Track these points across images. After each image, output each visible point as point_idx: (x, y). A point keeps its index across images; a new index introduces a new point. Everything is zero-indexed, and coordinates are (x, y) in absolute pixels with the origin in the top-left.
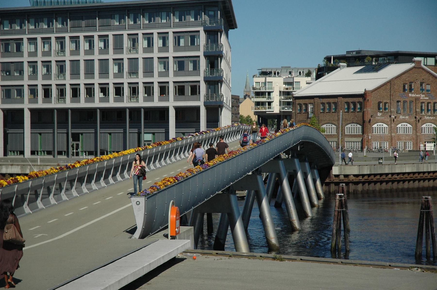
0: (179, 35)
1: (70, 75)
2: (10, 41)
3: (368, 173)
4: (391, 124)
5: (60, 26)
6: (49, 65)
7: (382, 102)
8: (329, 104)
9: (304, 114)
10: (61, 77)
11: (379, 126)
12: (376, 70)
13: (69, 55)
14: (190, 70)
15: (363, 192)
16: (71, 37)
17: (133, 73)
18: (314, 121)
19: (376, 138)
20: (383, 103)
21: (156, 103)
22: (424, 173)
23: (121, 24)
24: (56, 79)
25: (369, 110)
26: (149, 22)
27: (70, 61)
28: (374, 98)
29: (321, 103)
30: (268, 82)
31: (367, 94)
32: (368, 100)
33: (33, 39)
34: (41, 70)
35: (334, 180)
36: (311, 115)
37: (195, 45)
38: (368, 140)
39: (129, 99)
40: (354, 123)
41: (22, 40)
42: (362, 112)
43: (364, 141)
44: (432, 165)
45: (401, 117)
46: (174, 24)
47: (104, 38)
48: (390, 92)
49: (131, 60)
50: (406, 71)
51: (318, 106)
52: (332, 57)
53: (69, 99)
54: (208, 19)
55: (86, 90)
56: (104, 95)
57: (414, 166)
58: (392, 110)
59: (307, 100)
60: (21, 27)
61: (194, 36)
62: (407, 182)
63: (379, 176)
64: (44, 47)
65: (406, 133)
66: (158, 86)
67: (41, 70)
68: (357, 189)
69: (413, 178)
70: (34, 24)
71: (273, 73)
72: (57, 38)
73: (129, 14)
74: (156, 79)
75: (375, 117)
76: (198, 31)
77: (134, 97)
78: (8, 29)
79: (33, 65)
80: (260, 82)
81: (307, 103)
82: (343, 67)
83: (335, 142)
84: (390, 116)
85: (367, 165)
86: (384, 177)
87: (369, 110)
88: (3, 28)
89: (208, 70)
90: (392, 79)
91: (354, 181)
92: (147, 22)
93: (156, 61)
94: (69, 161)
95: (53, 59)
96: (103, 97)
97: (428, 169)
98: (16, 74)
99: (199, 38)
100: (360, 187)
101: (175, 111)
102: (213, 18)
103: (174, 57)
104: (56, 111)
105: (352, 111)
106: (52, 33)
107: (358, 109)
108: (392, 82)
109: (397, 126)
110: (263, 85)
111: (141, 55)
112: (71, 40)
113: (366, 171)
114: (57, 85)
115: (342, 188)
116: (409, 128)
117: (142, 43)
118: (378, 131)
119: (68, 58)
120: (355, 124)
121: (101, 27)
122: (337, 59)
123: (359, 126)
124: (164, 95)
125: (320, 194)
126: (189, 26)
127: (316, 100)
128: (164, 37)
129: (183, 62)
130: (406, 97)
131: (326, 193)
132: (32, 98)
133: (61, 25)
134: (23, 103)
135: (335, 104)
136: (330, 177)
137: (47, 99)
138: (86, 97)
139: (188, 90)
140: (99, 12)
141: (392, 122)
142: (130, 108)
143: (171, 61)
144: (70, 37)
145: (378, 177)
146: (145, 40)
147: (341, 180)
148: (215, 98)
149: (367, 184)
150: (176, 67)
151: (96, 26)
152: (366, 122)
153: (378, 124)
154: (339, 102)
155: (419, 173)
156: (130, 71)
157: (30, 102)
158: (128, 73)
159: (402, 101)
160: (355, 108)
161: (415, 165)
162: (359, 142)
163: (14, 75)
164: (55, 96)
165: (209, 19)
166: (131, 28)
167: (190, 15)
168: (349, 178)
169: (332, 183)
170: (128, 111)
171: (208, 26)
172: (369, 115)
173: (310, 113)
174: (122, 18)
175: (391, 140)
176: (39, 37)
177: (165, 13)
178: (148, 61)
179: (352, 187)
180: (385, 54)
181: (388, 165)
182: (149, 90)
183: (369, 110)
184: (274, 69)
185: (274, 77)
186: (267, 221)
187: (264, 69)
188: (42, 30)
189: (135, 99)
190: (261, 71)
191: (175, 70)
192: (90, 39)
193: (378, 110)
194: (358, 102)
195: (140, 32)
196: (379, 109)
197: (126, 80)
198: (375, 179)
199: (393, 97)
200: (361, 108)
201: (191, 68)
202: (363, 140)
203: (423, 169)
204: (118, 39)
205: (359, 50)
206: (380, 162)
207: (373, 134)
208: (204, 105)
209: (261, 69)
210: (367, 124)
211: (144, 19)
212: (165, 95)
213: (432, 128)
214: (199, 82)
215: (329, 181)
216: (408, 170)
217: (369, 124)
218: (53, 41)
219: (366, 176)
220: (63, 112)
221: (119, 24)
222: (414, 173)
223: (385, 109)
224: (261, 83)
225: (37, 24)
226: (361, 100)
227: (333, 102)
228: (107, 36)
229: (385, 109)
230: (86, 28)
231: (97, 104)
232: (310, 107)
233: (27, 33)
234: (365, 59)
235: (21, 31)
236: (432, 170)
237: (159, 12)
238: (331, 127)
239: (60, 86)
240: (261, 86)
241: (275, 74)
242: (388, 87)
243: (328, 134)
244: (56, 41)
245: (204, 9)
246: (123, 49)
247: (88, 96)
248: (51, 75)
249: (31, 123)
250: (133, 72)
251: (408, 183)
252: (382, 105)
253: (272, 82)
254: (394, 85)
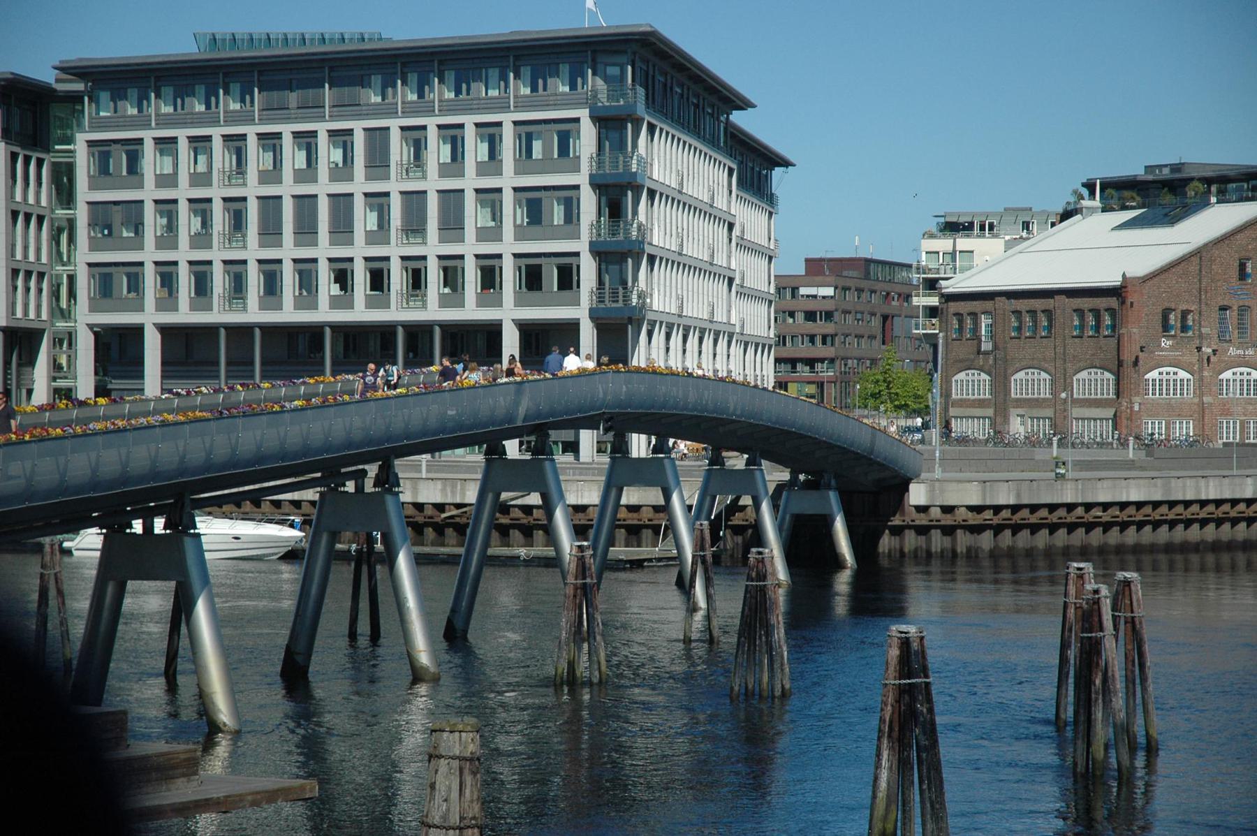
0: (530, 131)
1: (257, 236)
2: (110, 145)
3: (1012, 502)
4: (1201, 370)
5: (235, 106)
6: (574, 198)
7: (1174, 310)
8: (1097, 313)
9: (969, 342)
10: (237, 241)
11: (1165, 377)
12: (1172, 221)
13: (436, 177)
14: (556, 223)
15: (994, 555)
16: (261, 136)
17: (413, 231)
18: (890, 361)
19: (1155, 410)
20: (1179, 311)
21: (471, 311)
22: (1187, 504)
23: (386, 101)
24: (225, 248)
25: (1134, 332)
26: (456, 95)
27: (329, 195)
28: (1149, 297)
29: (1013, 312)
30: (960, 252)
31: (1129, 289)
32: (1132, 303)
33: (133, 142)
34: (187, 223)
35: (913, 521)
36: (986, 346)
37: (569, 155)
38: (1131, 414)
39: (404, 300)
40: (1095, 367)
41: (315, 134)
42: (1117, 336)
43: (1120, 417)
44: (1211, 484)
45: (1232, 351)
46: (441, 104)
47: (342, 138)
48: (1200, 281)
49: (336, 198)
50: (1247, 222)
51: (1004, 320)
52: (1098, 181)
53: (257, 299)
54: (602, 87)
55: (297, 276)
56: (341, 290)
57: (1155, 486)
58: (1204, 330)
59: (977, 302)
60: (421, 95)
61: (566, 134)
62: (1133, 528)
63: (1047, 510)
64: (196, 162)
65: (1227, 394)
66: (477, 266)
67: (187, 223)
68: (979, 545)
69: (1181, 517)
70: (172, 103)
71: (976, 227)
72: (227, 138)
73: (160, 87)
74: (470, 247)
75: (1153, 352)
76: (577, 120)
77: (417, 296)
78: (109, 114)
79: (167, 207)
80: (938, 253)
81: (977, 310)
82: (1092, 210)
83: (1048, 418)
84: (1197, 348)
85: (1007, 481)
86: (1062, 512)
87: (1135, 330)
88: (98, 113)
89: (605, 222)
90: (1206, 245)
91: (971, 522)
92: (527, 91)
93: (470, 198)
94: (571, 471)
95: (216, 192)
96: (340, 295)
97: (1199, 492)
98: (125, 234)
99: (579, 138)
100: (986, 540)
101: (518, 333)
102: (616, 83)
103: (515, 189)
104: (222, 331)
105: (1091, 333)
106: (320, 119)
107: (1107, 329)
108: (1204, 254)
109: (1221, 377)
110: (948, 258)
111: (433, 183)
112: (262, 142)
113: (1005, 497)
114: (403, 258)
115: (699, 532)
116: (1182, 380)
117: (438, 152)
118: (979, 385)
119: (252, 189)
120: (1099, 371)
121: (335, 109)
122: (1113, 188)
123: (1108, 375)
124: (492, 290)
125: (844, 555)
126: (556, 106)
127: (1001, 301)
128: (490, 132)
129: (539, 201)
130: (1247, 294)
131: (893, 554)
132: (165, 298)
133: (239, 104)
134: (141, 309)
135: (1049, 313)
136: (903, 514)
137: (202, 300)
138: (297, 294)
139: (551, 277)
140: (332, 69)
141: (1204, 368)
142: (406, 324)
143: (508, 198)
144: (328, 131)
145: (1044, 513)
146: (444, 144)
147: (932, 521)
148: (621, 298)
149: (1008, 532)
150: (522, 217)
151: (324, 107)
152: (1125, 366)
153: (1161, 370)
154: (1058, 311)
155: (1172, 504)
156: (406, 226)
157: (161, 306)
158: (402, 230)
159: (1235, 308)
160: (1098, 327)
161: (1159, 482)
162: (1107, 419)
163: (122, 237)
164: (221, 291)
165: (605, 87)
166: (409, 111)
167: (558, 77)
168: (954, 516)
169: (909, 527)
170: (400, 332)
171: (604, 107)
172: (1133, 346)
173: (983, 339)
174: (388, 83)
175: (1201, 412)
176: (182, 134)
177: (497, 70)
178: (451, 200)
179: (964, 539)
180: (1243, 175)
181: (1074, 483)
182: (452, 274)
183: (1135, 330)
184: (981, 214)
185: (978, 236)
186: (408, 608)
187: (952, 214)
188: (191, 116)
189: (419, 301)
190: (942, 220)
191: (519, 222)
192: (306, 140)
193: (1161, 330)
194: (1107, 310)
195: (431, 122)
196: (1166, 327)
197: (395, 250)
198: (1034, 519)
199: (1209, 295)
200: (1114, 327)
201: (559, 219)
202: (1118, 414)
203: (1184, 494)
204: (378, 138)
205: (1180, 164)
206: (1059, 473)
207: (1147, 399)
208: (590, 318)
209: (943, 214)
210: (1128, 370)
211: (520, 83)
212: (494, 289)
213: (1252, 383)
214: (577, 254)
215: (901, 523)
216: (1135, 496)
217: (1136, 372)
218: (217, 144)
219: (1004, 511)
220: (240, 333)
221: (383, 99)
222: (1156, 505)
223: (1184, 328)
224: (941, 254)
225: (179, 101)
226: (1113, 302)
227: (1043, 308)
228: (350, 132)
229: (1184, 328)
230: (300, 111)
231: (324, 313)
232: (985, 322)
233: (153, 124)
234: (1187, 189)
235: (535, 99)
236: (1212, 497)
237: (481, 68)
238: (979, 378)
239: (523, 259)
240: (941, 261)
241: (982, 228)
242: (1193, 267)
243: (1030, 396)
244: (224, 146)
245: (594, 60)
246: (389, 166)
247: (305, 293)
248: (212, 235)
249: (163, 364)
250: (415, 227)
251: (1138, 530)
252: (1176, 317)
253: (972, 252)
254: (1212, 261)
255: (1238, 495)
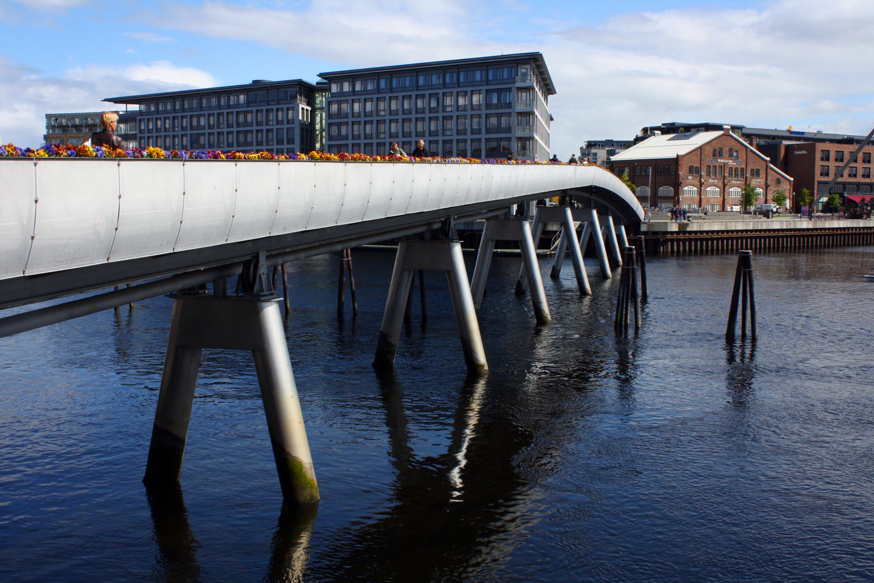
45: (711, 181)
57: (723, 225)
109: (707, 189)
155: (728, 232)
161: (724, 223)
222: (722, 232)
236: (740, 229)
255: (748, 228)
